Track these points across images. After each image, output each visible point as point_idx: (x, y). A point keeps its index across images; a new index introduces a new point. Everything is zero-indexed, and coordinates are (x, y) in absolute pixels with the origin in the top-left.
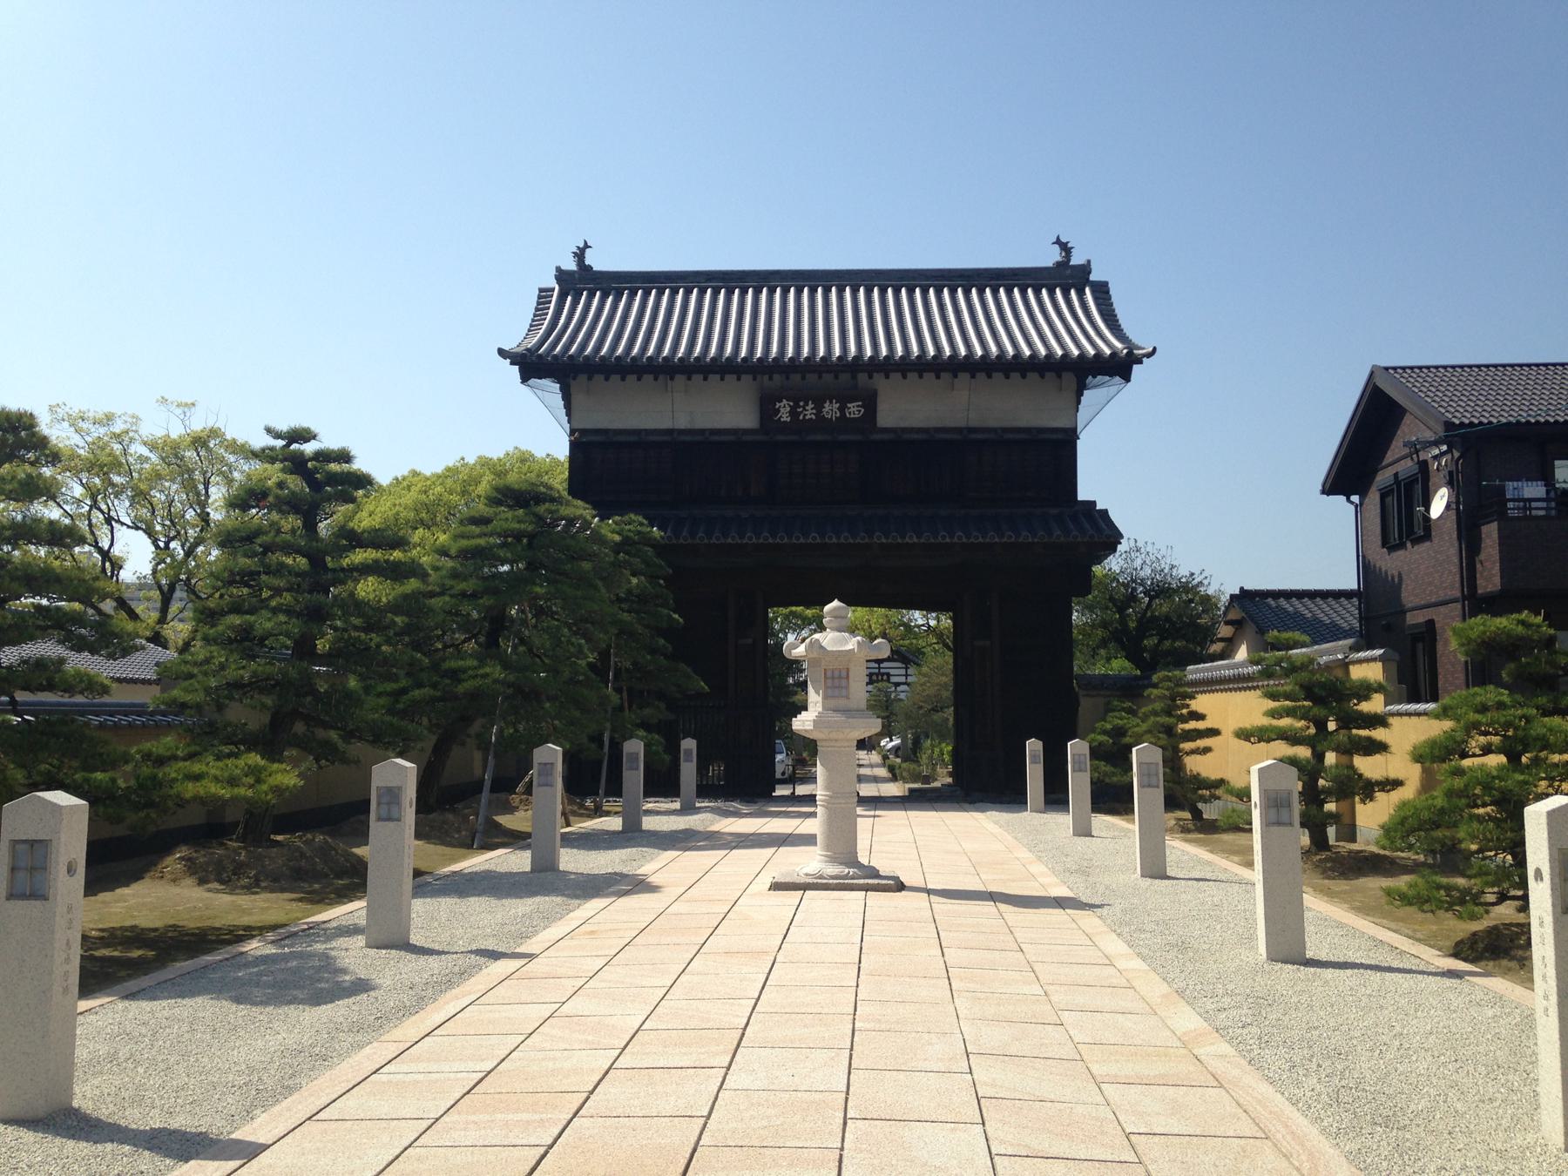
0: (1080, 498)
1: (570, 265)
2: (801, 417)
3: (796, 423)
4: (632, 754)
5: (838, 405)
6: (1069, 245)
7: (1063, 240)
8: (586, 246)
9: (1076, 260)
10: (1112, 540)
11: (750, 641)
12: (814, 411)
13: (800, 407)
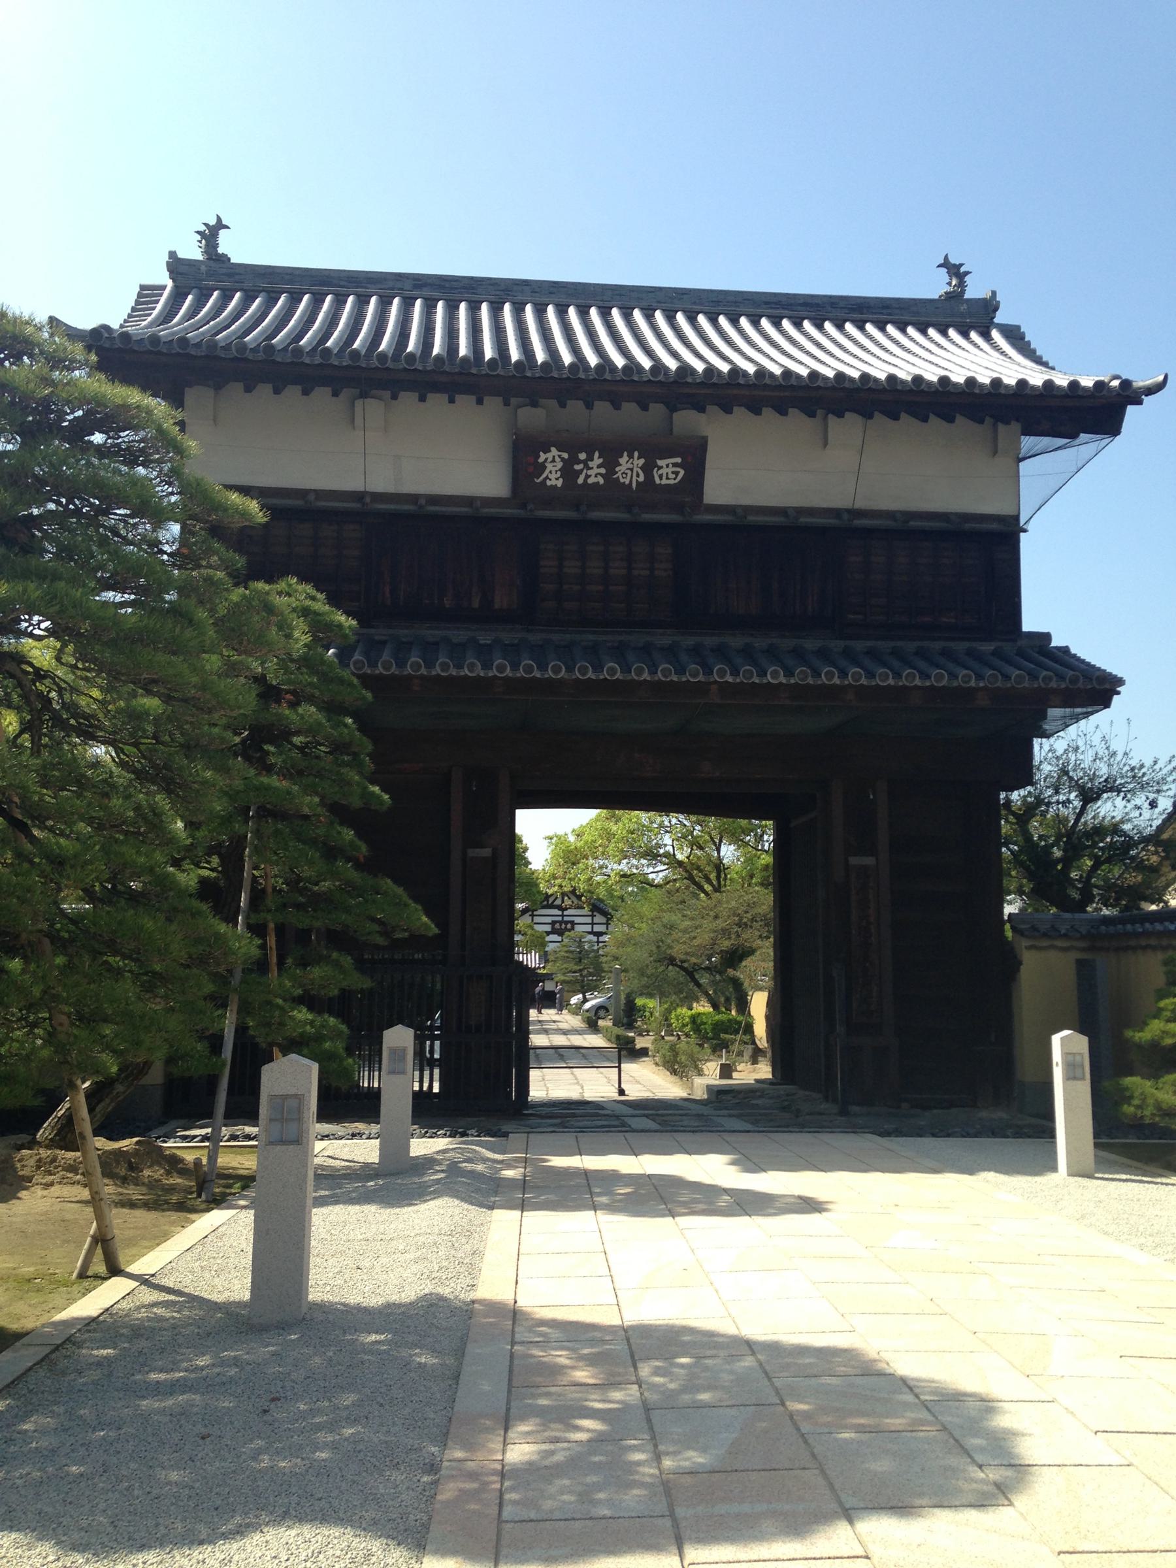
2: (580, 481)
4: (285, 1097)
5: (642, 461)
6: (962, 270)
7: (953, 260)
8: (220, 225)
9: (975, 290)
10: (1107, 686)
11: (486, 852)
12: (603, 471)
13: (579, 462)
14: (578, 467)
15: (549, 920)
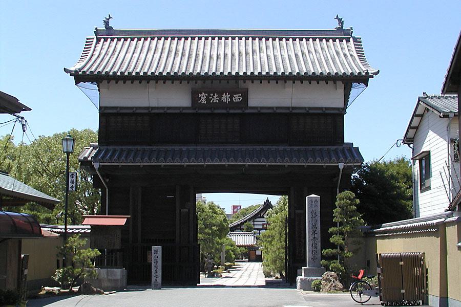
0: (345, 142)
1: (102, 27)
3: (209, 104)
7: (340, 17)
11: (187, 210)
12: (218, 98)
14: (211, 98)
15: (261, 223)
